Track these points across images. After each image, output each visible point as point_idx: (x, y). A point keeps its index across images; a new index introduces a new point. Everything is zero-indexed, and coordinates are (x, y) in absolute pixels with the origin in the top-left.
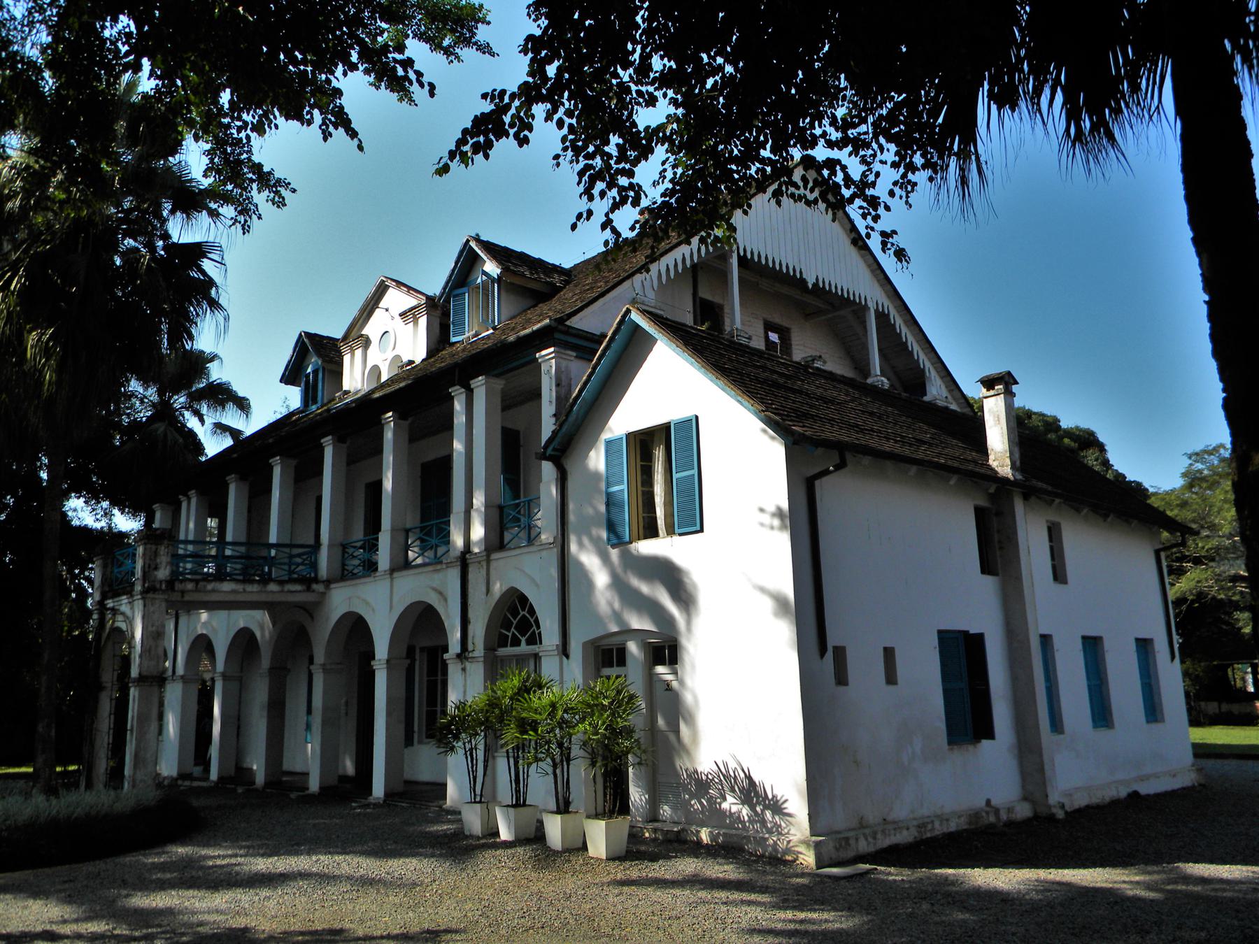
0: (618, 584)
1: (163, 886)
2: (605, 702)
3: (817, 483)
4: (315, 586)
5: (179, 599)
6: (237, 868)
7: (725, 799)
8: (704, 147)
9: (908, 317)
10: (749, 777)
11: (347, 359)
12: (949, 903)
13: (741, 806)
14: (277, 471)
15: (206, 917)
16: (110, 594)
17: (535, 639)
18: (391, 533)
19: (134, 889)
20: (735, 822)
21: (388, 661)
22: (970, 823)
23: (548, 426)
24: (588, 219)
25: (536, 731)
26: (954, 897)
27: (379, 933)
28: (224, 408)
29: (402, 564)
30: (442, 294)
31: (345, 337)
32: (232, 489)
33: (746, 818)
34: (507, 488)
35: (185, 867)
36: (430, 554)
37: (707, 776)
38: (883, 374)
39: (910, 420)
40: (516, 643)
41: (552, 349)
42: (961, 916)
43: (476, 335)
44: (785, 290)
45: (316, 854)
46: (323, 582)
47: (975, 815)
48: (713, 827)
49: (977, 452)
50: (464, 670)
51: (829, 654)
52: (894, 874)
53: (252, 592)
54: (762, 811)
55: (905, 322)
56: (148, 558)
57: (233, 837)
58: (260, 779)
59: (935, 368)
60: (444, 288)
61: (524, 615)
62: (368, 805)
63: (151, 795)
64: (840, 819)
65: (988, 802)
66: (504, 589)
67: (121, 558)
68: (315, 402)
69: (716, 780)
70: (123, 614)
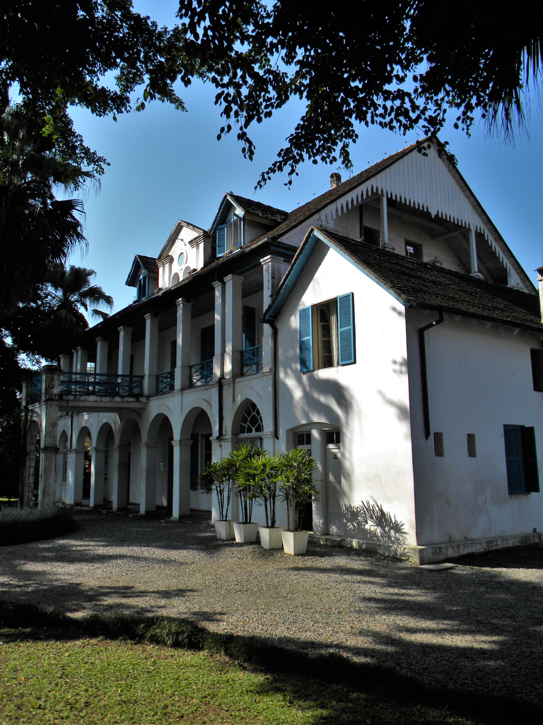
0: (307, 396)
1: (45, 560)
2: (295, 464)
3: (426, 332)
4: (141, 399)
5: (66, 405)
6: (88, 552)
7: (367, 523)
8: (320, 92)
9: (497, 236)
10: (381, 511)
11: (161, 270)
12: (498, 587)
13: (376, 527)
14: (122, 334)
15: (62, 577)
16: (30, 402)
17: (259, 429)
18: (182, 369)
19: (29, 561)
20: (373, 536)
21: (180, 441)
22: (522, 542)
23: (267, 301)
24: (228, 131)
25: (254, 480)
26: (502, 584)
27: (150, 590)
28: (99, 302)
29: (189, 385)
30: (212, 228)
31: (160, 257)
32: (99, 345)
33: (379, 534)
34: (247, 341)
35: (60, 550)
36: (204, 381)
37: (357, 509)
38: (479, 271)
39: (491, 296)
40: (250, 431)
41: (269, 256)
42: (503, 596)
43: (231, 252)
44: (417, 220)
45: (133, 546)
46: (146, 396)
47: (526, 538)
48: (359, 539)
49: (534, 315)
50: (221, 446)
51: (432, 437)
52: (462, 570)
53: (106, 402)
54: (389, 530)
55: (495, 239)
56: (48, 381)
57: (91, 535)
58: (115, 506)
59: (514, 268)
60: (213, 225)
61: (254, 415)
62: (170, 522)
63: (50, 511)
64: (437, 537)
65: (535, 530)
66: (243, 399)
67: (36, 382)
68: (144, 295)
69: (362, 512)
70: (36, 413)
